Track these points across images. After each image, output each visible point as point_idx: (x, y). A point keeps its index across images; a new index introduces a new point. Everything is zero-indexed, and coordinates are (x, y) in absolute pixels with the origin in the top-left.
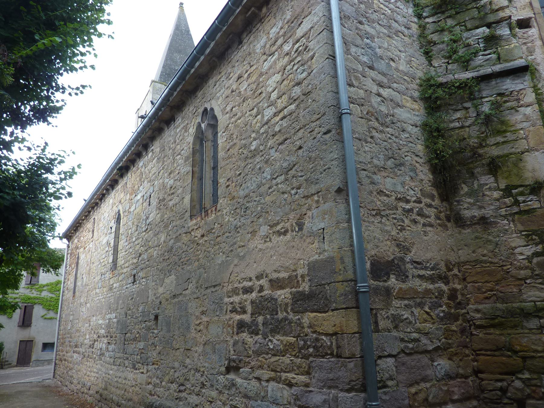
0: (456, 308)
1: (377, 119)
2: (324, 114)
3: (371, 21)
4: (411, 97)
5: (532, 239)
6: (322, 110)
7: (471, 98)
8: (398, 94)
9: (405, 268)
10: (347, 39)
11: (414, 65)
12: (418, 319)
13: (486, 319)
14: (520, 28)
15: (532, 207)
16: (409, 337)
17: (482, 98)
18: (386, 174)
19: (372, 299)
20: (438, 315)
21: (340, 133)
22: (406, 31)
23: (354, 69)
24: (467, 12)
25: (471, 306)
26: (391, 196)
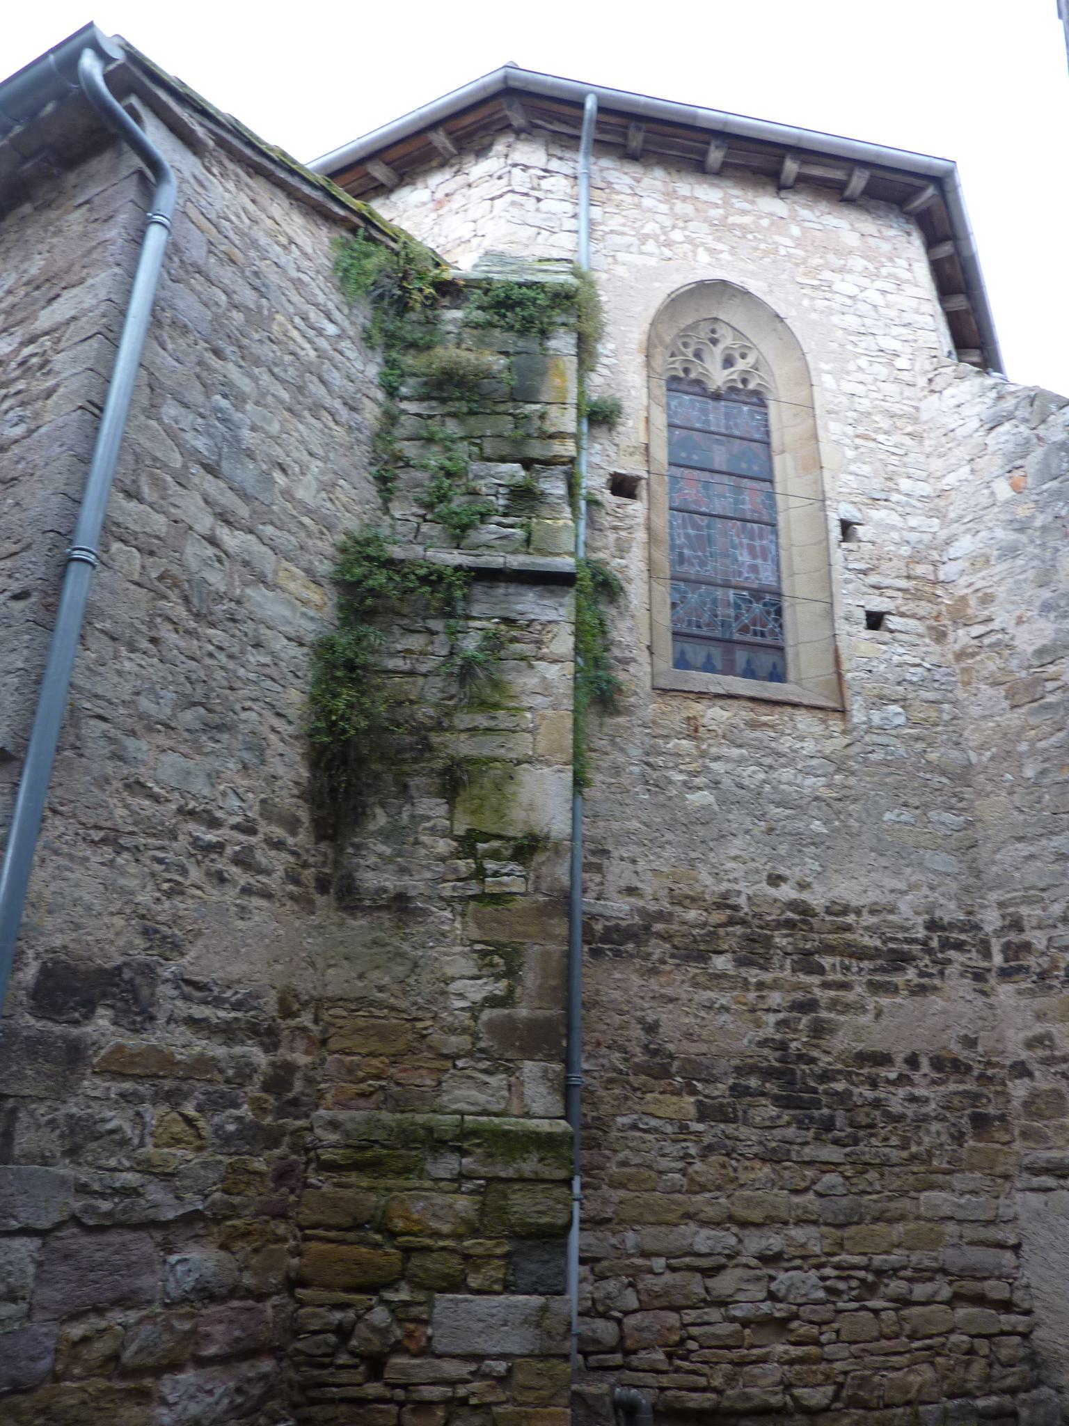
0: (281, 1113)
1: (186, 599)
2: (28, 547)
3: (248, 358)
4: (308, 571)
5: (491, 965)
6: (29, 534)
7: (448, 611)
8: (270, 552)
9: (153, 994)
10: (162, 379)
11: (341, 496)
12: (152, 1134)
13: (348, 1146)
14: (614, 493)
15: (508, 890)
16: (108, 1182)
17: (469, 618)
18: (168, 743)
19: (15, 1068)
20: (218, 1129)
21: (52, 608)
22: (344, 413)
23: (155, 459)
24: (493, 418)
25: (322, 1112)
26: (168, 801)
